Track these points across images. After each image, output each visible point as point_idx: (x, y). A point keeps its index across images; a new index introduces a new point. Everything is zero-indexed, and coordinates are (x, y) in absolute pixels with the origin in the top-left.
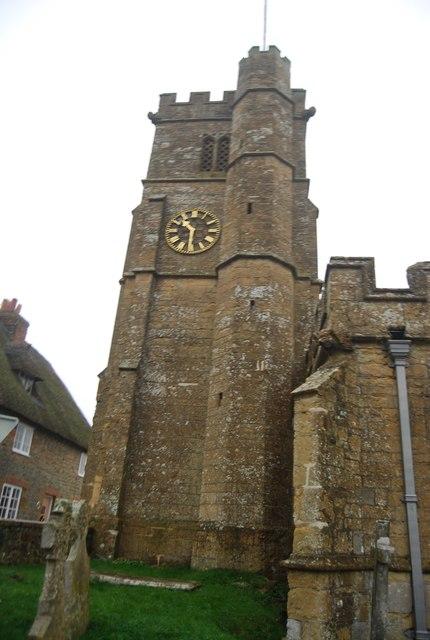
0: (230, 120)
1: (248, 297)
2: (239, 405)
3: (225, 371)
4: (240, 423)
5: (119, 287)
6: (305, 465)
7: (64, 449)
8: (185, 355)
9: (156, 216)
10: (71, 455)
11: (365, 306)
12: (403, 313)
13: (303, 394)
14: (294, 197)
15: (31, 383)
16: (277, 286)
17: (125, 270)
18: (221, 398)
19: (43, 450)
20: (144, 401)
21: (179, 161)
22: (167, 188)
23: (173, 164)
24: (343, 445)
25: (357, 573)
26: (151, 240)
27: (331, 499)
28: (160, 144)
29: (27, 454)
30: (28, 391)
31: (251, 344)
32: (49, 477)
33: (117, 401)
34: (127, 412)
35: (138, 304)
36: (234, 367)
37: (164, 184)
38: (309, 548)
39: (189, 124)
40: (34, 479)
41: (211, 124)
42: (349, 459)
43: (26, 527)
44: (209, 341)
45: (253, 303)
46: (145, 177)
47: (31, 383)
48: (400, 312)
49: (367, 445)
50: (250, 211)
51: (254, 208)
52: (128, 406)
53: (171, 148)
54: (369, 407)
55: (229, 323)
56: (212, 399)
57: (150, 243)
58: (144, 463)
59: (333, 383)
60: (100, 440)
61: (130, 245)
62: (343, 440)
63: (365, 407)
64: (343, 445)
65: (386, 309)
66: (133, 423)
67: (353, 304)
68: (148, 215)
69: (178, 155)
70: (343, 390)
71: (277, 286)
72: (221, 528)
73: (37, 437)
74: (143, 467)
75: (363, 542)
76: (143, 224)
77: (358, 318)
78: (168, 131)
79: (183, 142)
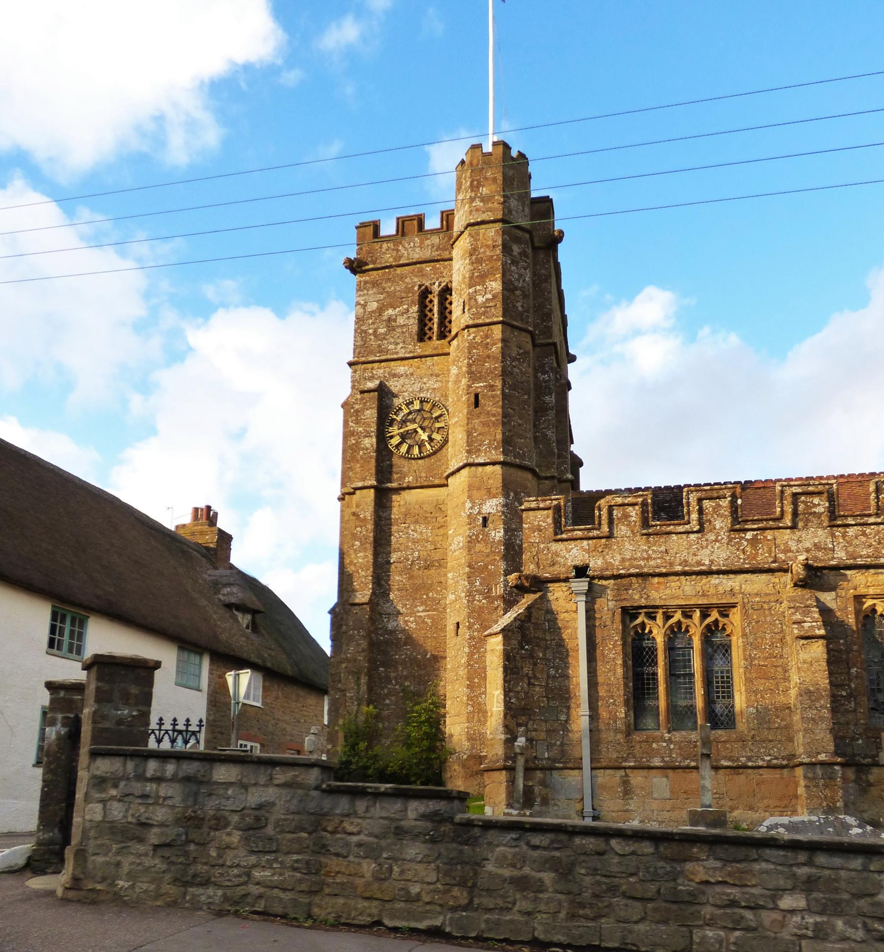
0: (451, 259)
1: (479, 513)
2: (476, 634)
3: (460, 598)
4: (478, 652)
5: (338, 504)
6: (494, 693)
7: (302, 693)
8: (420, 581)
9: (371, 415)
10: (311, 700)
11: (555, 547)
12: (588, 551)
13: (490, 635)
14: (536, 371)
15: (249, 617)
16: (512, 494)
17: (343, 485)
18: (458, 627)
19: (277, 698)
20: (381, 635)
21: (391, 329)
22: (380, 371)
23: (385, 334)
24: (528, 673)
25: (538, 772)
26: (368, 446)
27: (513, 717)
28: (364, 306)
29: (259, 704)
30: (247, 627)
31: (486, 566)
32: (289, 728)
33: (351, 638)
34: (363, 650)
35: (361, 527)
36: (470, 594)
37: (376, 365)
38: (497, 754)
39: (399, 270)
40: (272, 733)
41: (428, 268)
42: (534, 685)
43: (507, 304)
44: (441, 564)
45: (485, 520)
46: (350, 358)
47: (249, 617)
48: (585, 550)
49: (552, 672)
50: (477, 404)
51: (482, 401)
52: (364, 644)
53: (381, 310)
54: (554, 640)
55: (461, 544)
56: (451, 628)
57: (367, 449)
58: (387, 701)
59: (518, 623)
60: (340, 681)
61: (344, 451)
62: (527, 670)
63: (551, 640)
64: (528, 673)
65: (572, 548)
66: (372, 661)
67: (542, 546)
68: (362, 410)
69: (389, 320)
70: (528, 629)
71: (512, 494)
72: (465, 757)
73: (267, 684)
74: (388, 705)
75: (548, 749)
76: (357, 422)
77: (547, 560)
78: (375, 284)
79: (393, 301)
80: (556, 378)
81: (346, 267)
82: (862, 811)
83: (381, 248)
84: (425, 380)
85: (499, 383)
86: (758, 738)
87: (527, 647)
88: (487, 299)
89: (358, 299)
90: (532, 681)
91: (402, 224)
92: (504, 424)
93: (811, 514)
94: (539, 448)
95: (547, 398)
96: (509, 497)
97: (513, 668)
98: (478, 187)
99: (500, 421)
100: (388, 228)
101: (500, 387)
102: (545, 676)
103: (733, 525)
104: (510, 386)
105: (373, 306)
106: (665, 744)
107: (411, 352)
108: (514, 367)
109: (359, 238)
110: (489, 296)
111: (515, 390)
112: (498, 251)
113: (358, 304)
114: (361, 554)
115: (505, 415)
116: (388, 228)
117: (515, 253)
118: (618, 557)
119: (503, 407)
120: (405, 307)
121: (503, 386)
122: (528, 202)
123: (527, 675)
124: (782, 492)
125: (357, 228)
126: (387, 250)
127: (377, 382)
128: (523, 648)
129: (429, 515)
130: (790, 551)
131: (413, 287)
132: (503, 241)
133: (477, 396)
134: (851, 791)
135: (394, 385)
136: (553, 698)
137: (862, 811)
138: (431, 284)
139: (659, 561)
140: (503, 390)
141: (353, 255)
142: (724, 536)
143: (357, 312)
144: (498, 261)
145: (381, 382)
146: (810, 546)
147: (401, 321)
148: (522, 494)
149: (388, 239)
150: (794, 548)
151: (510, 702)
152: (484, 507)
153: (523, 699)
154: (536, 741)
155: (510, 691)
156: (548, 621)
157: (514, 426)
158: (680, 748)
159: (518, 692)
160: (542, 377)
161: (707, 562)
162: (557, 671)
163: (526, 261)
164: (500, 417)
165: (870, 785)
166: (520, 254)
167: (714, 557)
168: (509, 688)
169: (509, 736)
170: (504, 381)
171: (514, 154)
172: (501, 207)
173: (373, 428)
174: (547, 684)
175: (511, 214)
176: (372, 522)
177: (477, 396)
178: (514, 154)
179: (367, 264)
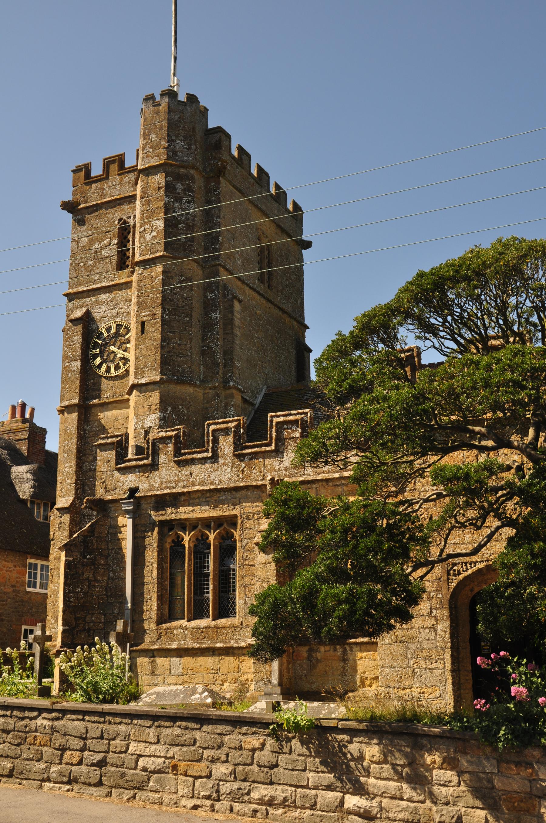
16: (170, 409)
26: (75, 368)
53: (90, 243)
57: (74, 371)
63: (112, 549)
71: (170, 409)
80: (225, 294)
81: (63, 209)
82: (312, 683)
83: (91, 188)
84: (121, 306)
85: (159, 311)
86: (244, 624)
87: (88, 557)
88: (153, 237)
89: (73, 236)
90: (93, 583)
91: (108, 163)
92: (162, 347)
93: (290, 438)
94: (206, 360)
95: (214, 315)
96: (166, 411)
97: (74, 574)
98: (149, 135)
99: (159, 346)
100: (97, 170)
101: (160, 315)
102: (106, 578)
103: (235, 450)
104: (169, 312)
105: (85, 241)
106: (182, 631)
107: (112, 281)
108: (175, 294)
109: (74, 181)
110: (154, 234)
111: (175, 315)
112: (162, 192)
113: (73, 240)
114: (68, 465)
115: (163, 340)
116: (97, 170)
117: (179, 191)
118: (159, 481)
119: (162, 333)
120: (108, 240)
121: (163, 313)
122: (199, 134)
123: (87, 579)
124: (272, 421)
125: (74, 171)
126: (96, 190)
127: (84, 310)
128: (85, 557)
129: (121, 426)
130: (275, 470)
131: (114, 221)
132: (166, 182)
133: (143, 323)
134: (304, 666)
135: (96, 315)
136: (111, 596)
137: (312, 683)
138: (128, 218)
139: (185, 483)
140: (162, 317)
141: (69, 197)
142: (229, 460)
143: (72, 247)
144: (162, 201)
145: (88, 310)
146: (288, 466)
147: (105, 253)
148: (180, 407)
149: (99, 179)
150: (277, 468)
151: (69, 601)
152: (146, 422)
153: (82, 598)
154: (94, 630)
155: (69, 592)
156: (111, 534)
157: (173, 347)
158: (192, 634)
159: (78, 593)
160: (210, 296)
161: (217, 482)
162: (114, 574)
163: (190, 195)
164: (159, 342)
165: (318, 661)
166: (184, 190)
167: (222, 478)
168: (69, 590)
169: (67, 628)
170: (164, 309)
171: (182, 97)
172: (165, 151)
173: (79, 352)
174: (108, 584)
175: (176, 155)
176: (75, 436)
177: (143, 323)
178: (182, 97)
179: (80, 204)
